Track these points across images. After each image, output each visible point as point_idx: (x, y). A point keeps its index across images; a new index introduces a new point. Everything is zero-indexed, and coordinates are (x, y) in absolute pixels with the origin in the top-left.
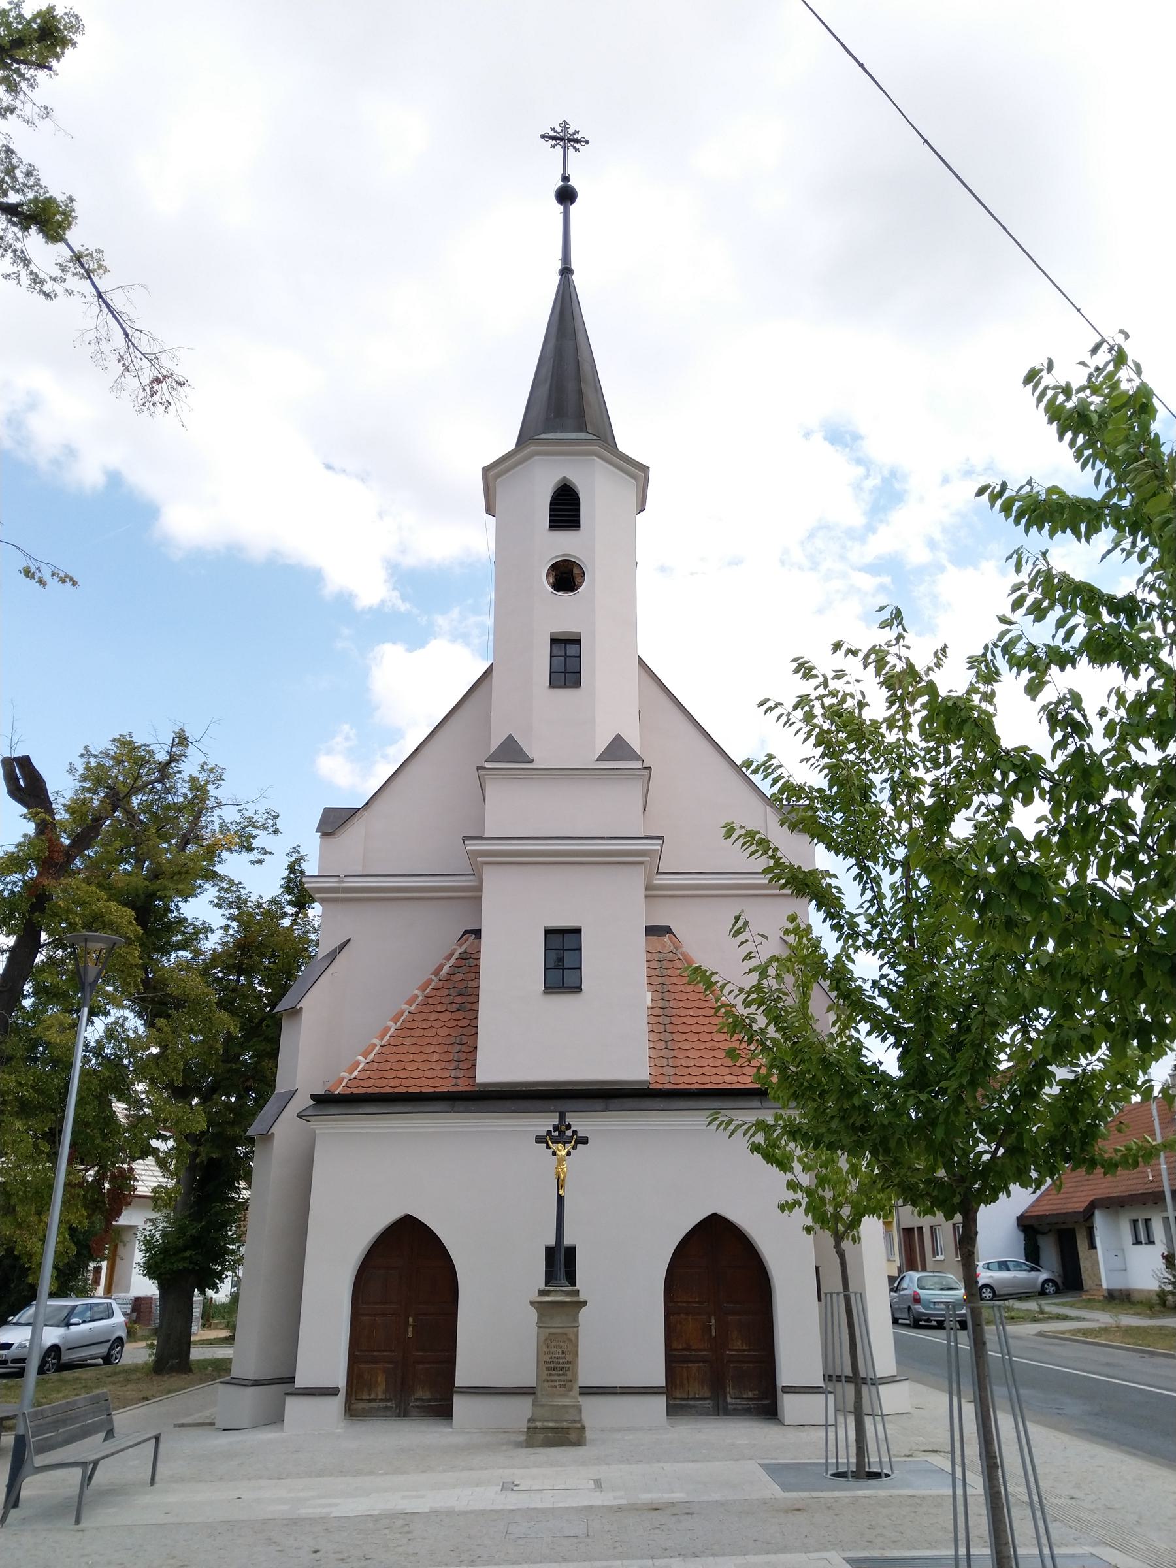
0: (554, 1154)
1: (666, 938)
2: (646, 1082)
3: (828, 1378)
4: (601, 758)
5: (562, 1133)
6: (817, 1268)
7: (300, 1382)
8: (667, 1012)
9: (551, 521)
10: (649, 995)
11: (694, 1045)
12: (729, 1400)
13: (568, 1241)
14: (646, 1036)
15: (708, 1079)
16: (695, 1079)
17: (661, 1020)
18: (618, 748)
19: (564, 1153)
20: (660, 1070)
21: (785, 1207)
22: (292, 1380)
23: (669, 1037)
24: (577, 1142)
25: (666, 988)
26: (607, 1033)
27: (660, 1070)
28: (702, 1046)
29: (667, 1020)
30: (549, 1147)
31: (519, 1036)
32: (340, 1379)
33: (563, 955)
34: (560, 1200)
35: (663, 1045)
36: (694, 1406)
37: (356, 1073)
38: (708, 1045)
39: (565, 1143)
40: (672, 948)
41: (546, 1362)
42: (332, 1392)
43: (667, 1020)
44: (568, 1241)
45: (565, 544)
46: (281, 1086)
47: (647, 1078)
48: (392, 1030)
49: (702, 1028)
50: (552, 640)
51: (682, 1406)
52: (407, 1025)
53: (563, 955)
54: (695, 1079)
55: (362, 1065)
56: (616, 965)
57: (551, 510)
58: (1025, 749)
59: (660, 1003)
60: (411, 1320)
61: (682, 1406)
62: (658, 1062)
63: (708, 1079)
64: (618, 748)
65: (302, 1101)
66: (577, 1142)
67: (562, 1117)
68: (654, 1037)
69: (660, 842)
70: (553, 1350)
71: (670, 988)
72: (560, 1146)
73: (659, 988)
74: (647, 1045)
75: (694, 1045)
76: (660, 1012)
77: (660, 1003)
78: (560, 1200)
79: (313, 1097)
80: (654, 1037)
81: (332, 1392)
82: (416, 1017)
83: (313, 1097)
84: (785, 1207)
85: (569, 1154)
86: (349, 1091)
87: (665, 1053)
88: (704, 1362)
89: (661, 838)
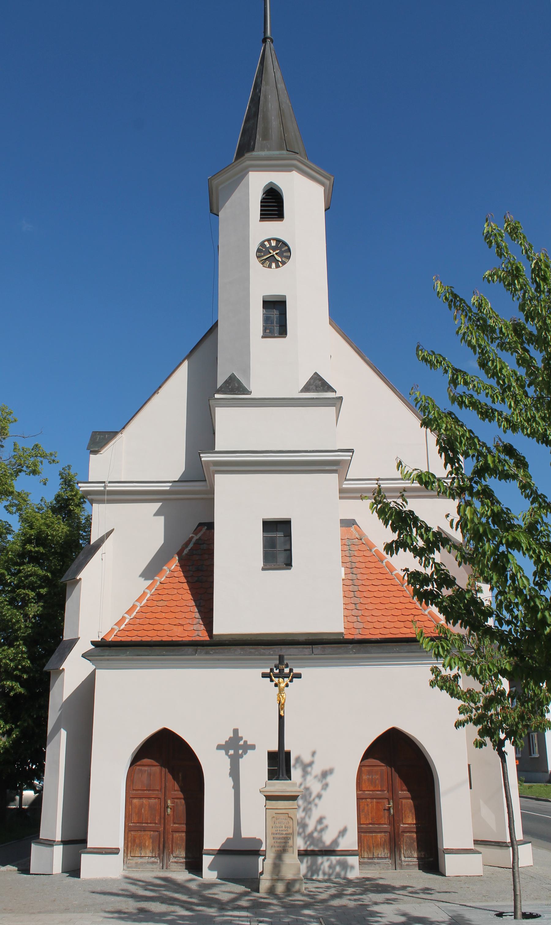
0: (276, 685)
1: (352, 529)
2: (342, 634)
3: (476, 842)
4: (306, 389)
5: (282, 671)
6: (469, 766)
7: (90, 844)
8: (356, 582)
9: (261, 214)
10: (343, 569)
11: (376, 606)
12: (403, 858)
13: (286, 748)
14: (341, 601)
15: (387, 631)
16: (378, 631)
17: (351, 588)
18: (317, 383)
19: (283, 685)
20: (351, 625)
21: (459, 724)
22: (84, 841)
23: (357, 600)
24: (293, 677)
25: (354, 565)
26: (311, 597)
27: (351, 625)
28: (383, 607)
29: (356, 588)
30: (272, 681)
31: (246, 598)
32: (120, 844)
33: (278, 537)
34: (281, 719)
35: (353, 606)
36: (378, 863)
37: (123, 627)
38: (387, 606)
39: (283, 677)
40: (357, 536)
41: (273, 834)
42: (114, 851)
43: (356, 588)
44: (286, 748)
45: (273, 229)
46: (67, 636)
47: (342, 630)
48: (148, 595)
49: (382, 594)
50: (264, 302)
51: (370, 863)
52: (159, 592)
53: (278, 537)
54: (378, 631)
55: (127, 621)
56: (317, 548)
57: (261, 206)
58: (493, 492)
59: (351, 576)
60: (169, 802)
61: (370, 863)
62: (350, 619)
63: (387, 631)
64: (317, 383)
65: (84, 645)
66: (293, 677)
67: (281, 659)
68: (348, 601)
69: (351, 454)
70: (278, 825)
71: (357, 565)
72: (281, 680)
73: (348, 565)
74: (342, 606)
75: (376, 606)
76: (350, 582)
77: (351, 576)
78: (281, 719)
79: (93, 643)
80: (348, 601)
81: (114, 851)
82: (165, 586)
83: (93, 643)
84: (459, 724)
85: (287, 685)
86: (119, 639)
87: (355, 612)
88: (385, 832)
89: (352, 451)
